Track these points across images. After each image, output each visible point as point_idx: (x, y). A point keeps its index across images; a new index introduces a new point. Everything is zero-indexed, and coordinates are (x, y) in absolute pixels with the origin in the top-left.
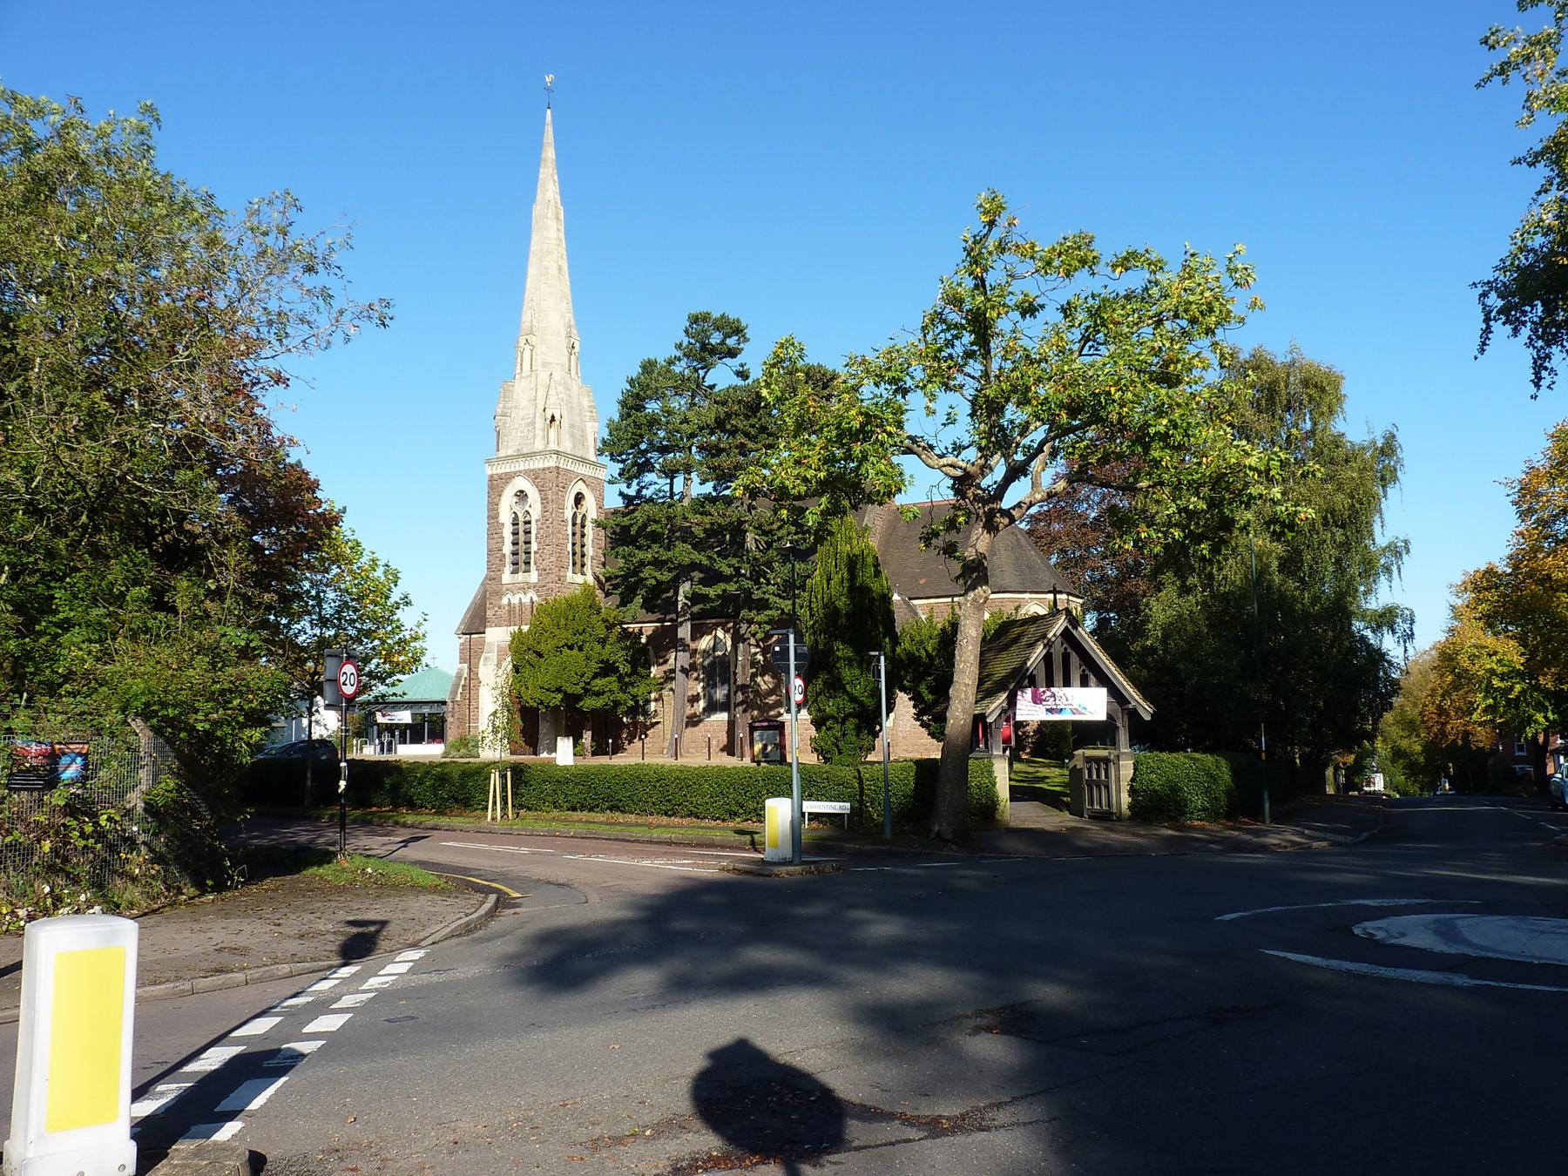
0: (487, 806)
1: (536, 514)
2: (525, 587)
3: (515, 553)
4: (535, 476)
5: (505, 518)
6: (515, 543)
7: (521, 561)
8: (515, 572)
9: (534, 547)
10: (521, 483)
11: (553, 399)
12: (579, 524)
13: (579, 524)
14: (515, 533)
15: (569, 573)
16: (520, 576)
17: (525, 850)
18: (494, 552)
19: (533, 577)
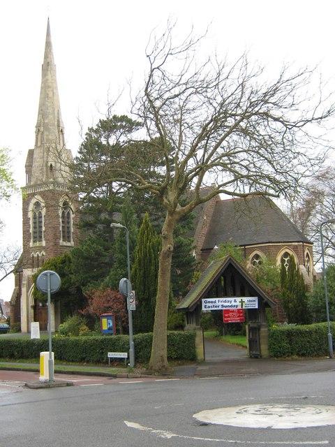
0: (326, 311)
1: (44, 212)
2: (41, 248)
3: (35, 232)
4: (43, 194)
5: (30, 215)
6: (35, 228)
7: (38, 237)
8: (34, 242)
9: (43, 229)
10: (38, 198)
11: (50, 159)
12: (66, 217)
13: (66, 217)
14: (35, 223)
15: (61, 241)
16: (38, 244)
17: (208, 368)
18: (26, 232)
19: (44, 243)
